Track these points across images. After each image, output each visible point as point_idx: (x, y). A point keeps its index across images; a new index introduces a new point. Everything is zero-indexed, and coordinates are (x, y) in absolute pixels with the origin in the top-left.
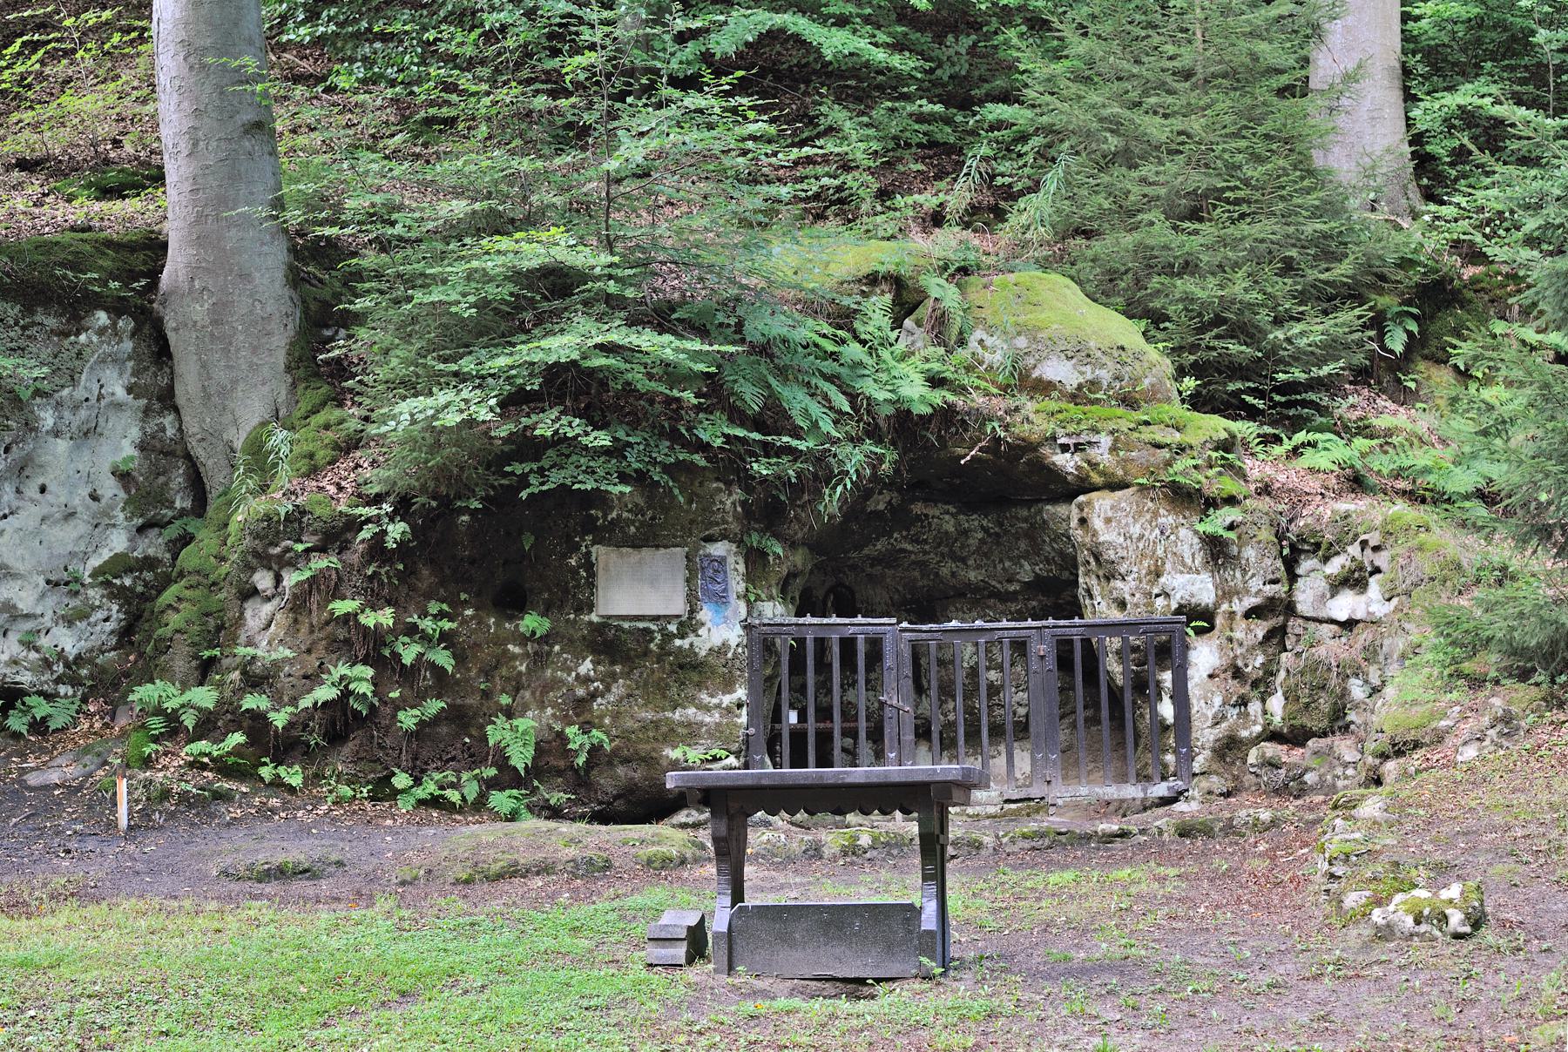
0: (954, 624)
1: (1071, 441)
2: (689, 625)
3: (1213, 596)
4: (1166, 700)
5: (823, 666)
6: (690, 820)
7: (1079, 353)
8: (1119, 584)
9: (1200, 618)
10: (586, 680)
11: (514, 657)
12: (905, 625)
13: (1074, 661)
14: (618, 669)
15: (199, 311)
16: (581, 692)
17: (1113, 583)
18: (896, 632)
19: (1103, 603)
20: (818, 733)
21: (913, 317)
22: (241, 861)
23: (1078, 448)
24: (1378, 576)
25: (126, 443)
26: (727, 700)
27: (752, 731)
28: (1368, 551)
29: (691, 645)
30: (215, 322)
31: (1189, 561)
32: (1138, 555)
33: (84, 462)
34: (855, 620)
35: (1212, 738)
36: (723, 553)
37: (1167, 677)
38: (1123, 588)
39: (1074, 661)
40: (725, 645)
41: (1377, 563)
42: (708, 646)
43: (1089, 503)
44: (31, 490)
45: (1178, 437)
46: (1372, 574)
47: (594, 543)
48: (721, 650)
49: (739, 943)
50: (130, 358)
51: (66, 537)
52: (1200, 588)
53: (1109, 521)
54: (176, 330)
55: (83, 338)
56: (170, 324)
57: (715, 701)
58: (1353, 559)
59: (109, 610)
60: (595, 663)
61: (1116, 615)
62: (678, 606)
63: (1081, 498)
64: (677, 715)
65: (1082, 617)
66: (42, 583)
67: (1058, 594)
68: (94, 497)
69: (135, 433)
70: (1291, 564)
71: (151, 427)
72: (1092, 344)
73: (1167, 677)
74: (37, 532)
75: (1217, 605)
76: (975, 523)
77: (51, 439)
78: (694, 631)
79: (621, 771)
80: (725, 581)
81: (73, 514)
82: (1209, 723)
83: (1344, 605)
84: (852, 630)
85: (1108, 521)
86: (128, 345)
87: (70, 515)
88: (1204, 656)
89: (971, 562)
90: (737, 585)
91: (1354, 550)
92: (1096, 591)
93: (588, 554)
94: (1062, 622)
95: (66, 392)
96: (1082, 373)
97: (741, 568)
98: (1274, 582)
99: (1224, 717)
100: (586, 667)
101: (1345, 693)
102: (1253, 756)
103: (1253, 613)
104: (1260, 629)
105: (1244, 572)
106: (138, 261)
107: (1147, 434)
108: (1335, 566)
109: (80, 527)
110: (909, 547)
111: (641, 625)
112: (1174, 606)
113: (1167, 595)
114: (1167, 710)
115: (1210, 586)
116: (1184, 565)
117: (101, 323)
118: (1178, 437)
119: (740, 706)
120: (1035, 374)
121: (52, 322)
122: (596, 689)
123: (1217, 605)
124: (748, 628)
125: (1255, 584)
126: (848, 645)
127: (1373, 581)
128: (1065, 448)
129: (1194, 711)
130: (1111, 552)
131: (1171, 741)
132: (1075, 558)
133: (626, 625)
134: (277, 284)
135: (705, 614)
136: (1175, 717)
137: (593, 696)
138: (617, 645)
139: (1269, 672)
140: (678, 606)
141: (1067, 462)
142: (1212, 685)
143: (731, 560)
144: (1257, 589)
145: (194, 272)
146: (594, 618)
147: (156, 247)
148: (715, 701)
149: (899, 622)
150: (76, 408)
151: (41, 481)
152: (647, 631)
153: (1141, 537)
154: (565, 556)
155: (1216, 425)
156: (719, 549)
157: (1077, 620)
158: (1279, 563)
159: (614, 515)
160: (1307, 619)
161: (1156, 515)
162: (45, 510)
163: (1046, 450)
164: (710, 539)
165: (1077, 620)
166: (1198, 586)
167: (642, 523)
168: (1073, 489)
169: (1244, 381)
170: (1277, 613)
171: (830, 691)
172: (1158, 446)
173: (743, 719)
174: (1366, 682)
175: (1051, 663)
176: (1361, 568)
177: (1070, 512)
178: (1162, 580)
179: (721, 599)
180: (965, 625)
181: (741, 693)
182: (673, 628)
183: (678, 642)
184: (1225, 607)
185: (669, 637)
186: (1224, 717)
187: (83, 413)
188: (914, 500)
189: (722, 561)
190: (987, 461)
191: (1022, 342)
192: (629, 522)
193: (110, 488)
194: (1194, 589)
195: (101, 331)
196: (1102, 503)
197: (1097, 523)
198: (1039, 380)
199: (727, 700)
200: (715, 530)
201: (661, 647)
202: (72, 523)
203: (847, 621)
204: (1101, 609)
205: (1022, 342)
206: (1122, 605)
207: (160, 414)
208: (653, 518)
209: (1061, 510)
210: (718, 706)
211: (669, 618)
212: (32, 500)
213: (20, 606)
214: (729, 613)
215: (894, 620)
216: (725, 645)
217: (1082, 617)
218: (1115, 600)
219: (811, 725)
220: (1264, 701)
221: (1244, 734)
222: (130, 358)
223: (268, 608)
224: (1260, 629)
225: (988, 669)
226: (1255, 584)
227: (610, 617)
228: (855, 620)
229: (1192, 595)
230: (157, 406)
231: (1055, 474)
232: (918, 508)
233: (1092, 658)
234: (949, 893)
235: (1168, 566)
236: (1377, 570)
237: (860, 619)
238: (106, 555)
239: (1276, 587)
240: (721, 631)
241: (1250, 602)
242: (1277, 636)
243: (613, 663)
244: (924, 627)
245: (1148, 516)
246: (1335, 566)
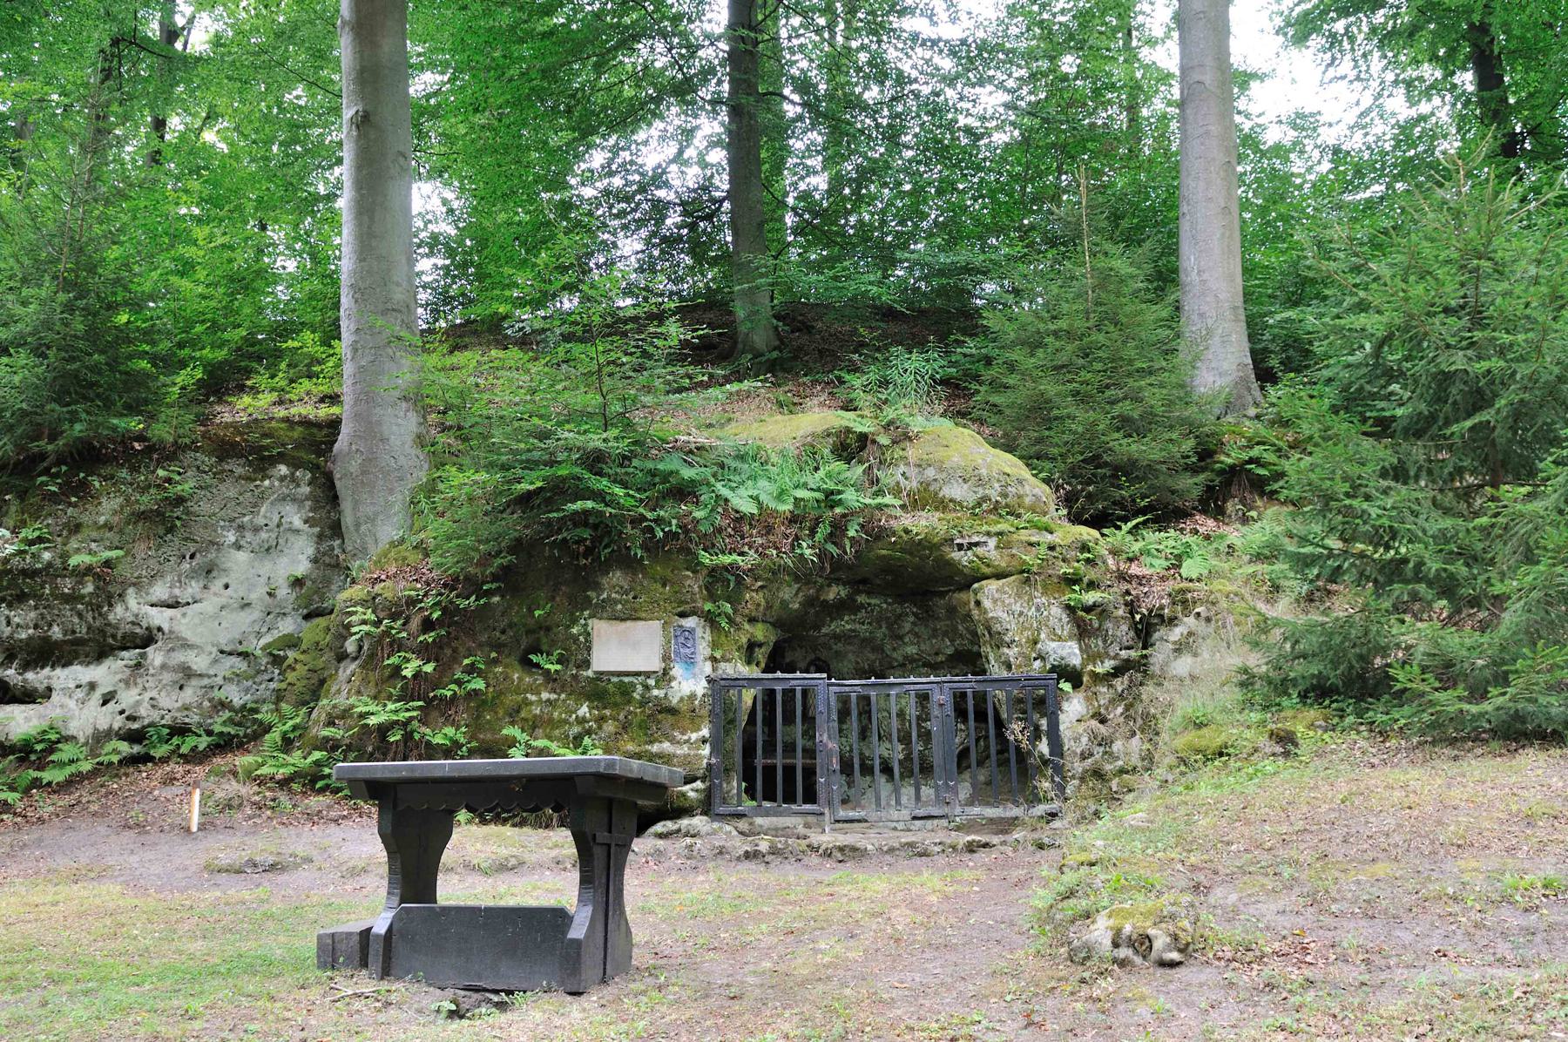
2: (665, 677)
4: (1044, 739)
6: (664, 830)
7: (973, 477)
8: (1006, 650)
11: (531, 703)
13: (974, 711)
15: (354, 466)
22: (225, 858)
25: (303, 558)
26: (694, 736)
27: (713, 761)
30: (364, 473)
32: (1024, 625)
33: (266, 568)
37: (1044, 723)
38: (1012, 653)
49: (399, 946)
50: (307, 499)
51: (245, 620)
52: (1070, 652)
53: (997, 602)
55: (267, 483)
56: (337, 476)
61: (1005, 674)
62: (655, 665)
66: (214, 650)
67: (969, 660)
69: (310, 551)
71: (324, 547)
73: (1044, 723)
74: (215, 617)
81: (248, 605)
85: (995, 601)
86: (305, 490)
87: (246, 605)
90: (703, 649)
93: (586, 625)
95: (246, 519)
100: (584, 710)
105: (1105, 641)
106: (320, 435)
109: (255, 614)
111: (626, 679)
112: (1048, 667)
113: (1043, 659)
115: (1077, 651)
121: (239, 471)
124: (710, 681)
126: (789, 694)
128: (960, 547)
133: (615, 679)
135: (677, 670)
138: (610, 693)
141: (964, 558)
143: (699, 632)
145: (356, 436)
146: (590, 673)
147: (334, 424)
150: (256, 530)
151: (225, 580)
152: (633, 685)
153: (1021, 614)
154: (569, 627)
162: (223, 601)
163: (947, 549)
169: (1104, 492)
171: (755, 724)
181: (705, 732)
183: (655, 692)
185: (647, 688)
187: (264, 535)
188: (859, 592)
189: (692, 631)
192: (616, 602)
193: (284, 591)
194: (1064, 653)
195: (282, 479)
196: (991, 586)
197: (987, 604)
199: (694, 736)
201: (643, 696)
202: (248, 610)
205: (930, 473)
206: (1009, 667)
207: (331, 538)
209: (963, 596)
211: (648, 674)
213: (195, 667)
222: (307, 499)
223: (353, 666)
230: (328, 532)
232: (861, 599)
235: (1043, 636)
237: (798, 675)
238: (276, 634)
240: (689, 684)
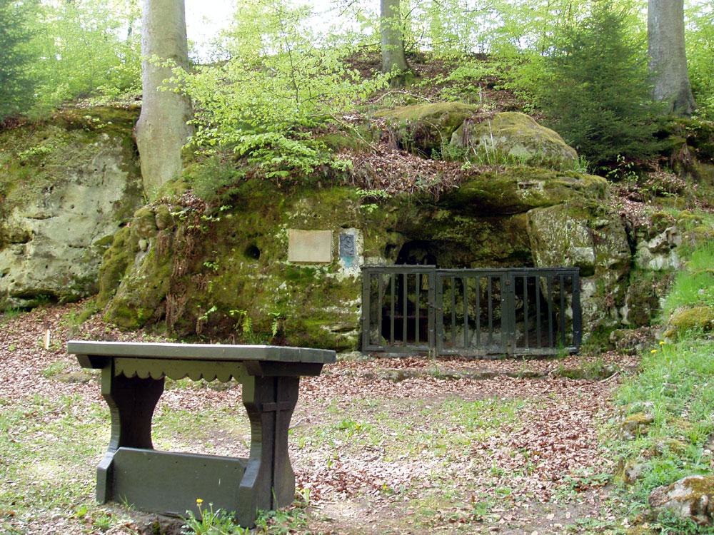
1: (524, 183)
2: (334, 267)
4: (570, 308)
7: (528, 143)
9: (586, 270)
20: (396, 320)
21: (456, 131)
24: (675, 249)
36: (352, 234)
37: (570, 297)
39: (525, 287)
40: (352, 278)
42: (343, 277)
44: (67, 206)
46: (672, 247)
47: (288, 227)
50: (121, 154)
54: (140, 142)
55: (96, 144)
56: (138, 141)
57: (347, 303)
59: (101, 258)
63: (530, 211)
64: (328, 309)
66: (66, 245)
68: (100, 211)
69: (123, 186)
73: (570, 297)
77: (76, 186)
80: (353, 246)
83: (658, 262)
84: (413, 270)
86: (120, 149)
88: (589, 287)
96: (531, 153)
97: (362, 241)
99: (598, 317)
100: (284, 285)
106: (128, 116)
108: (654, 243)
114: (569, 312)
117: (105, 139)
127: (672, 251)
131: (572, 328)
134: (179, 122)
135: (341, 262)
136: (573, 316)
140: (327, 257)
142: (592, 300)
148: (347, 303)
151: (72, 203)
152: (313, 270)
155: (599, 180)
156: (350, 232)
159: (297, 214)
164: (346, 227)
167: (310, 218)
168: (525, 208)
170: (628, 268)
173: (359, 312)
176: (667, 244)
177: (524, 217)
179: (350, 256)
181: (359, 300)
186: (598, 317)
189: (351, 237)
191: (504, 139)
195: (105, 142)
196: (541, 212)
200: (349, 223)
207: (135, 178)
208: (315, 216)
210: (348, 306)
212: (66, 211)
214: (354, 262)
216: (352, 278)
219: (405, 317)
221: (608, 325)
222: (121, 154)
225: (493, 293)
227: (295, 263)
232: (457, 218)
234: (275, 471)
239: (625, 254)
240: (349, 271)
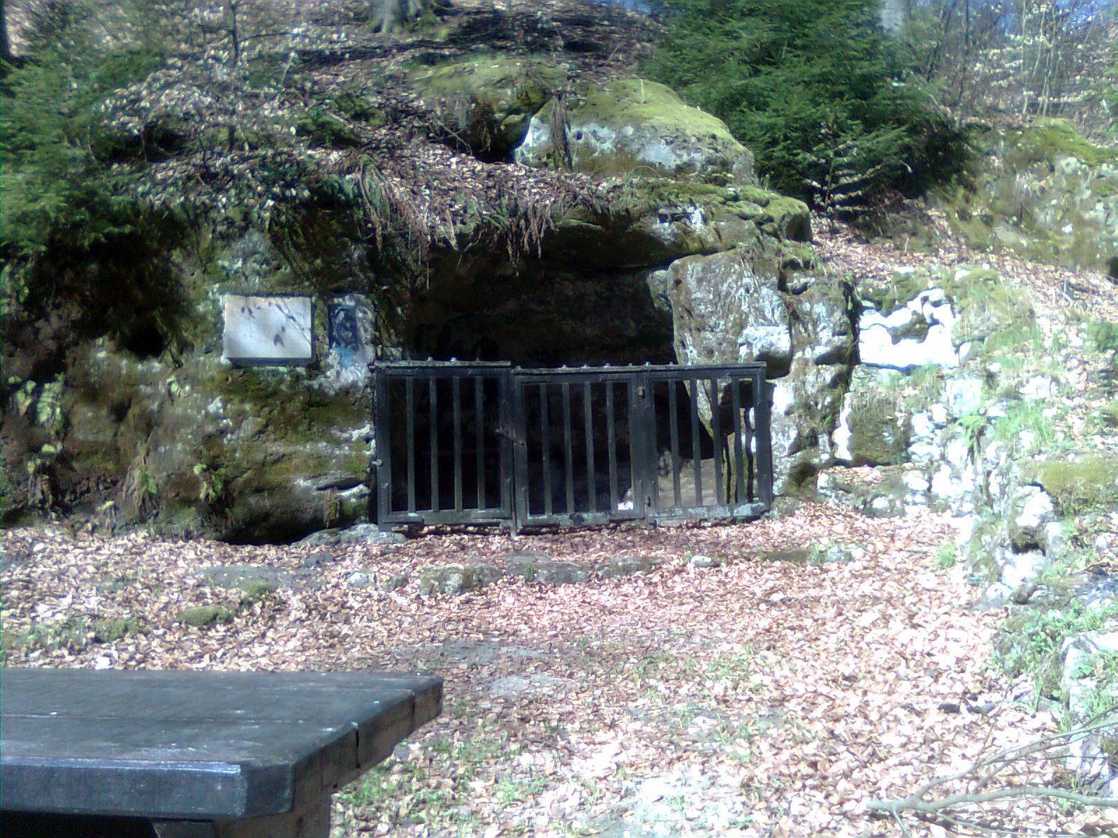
0: (564, 368)
3: (788, 345)
5: (468, 402)
7: (677, 140)
9: (777, 365)
10: (216, 418)
12: (519, 368)
14: (248, 407)
16: (210, 429)
17: (703, 334)
18: (517, 375)
19: (695, 352)
23: (675, 218)
27: (378, 462)
28: (927, 305)
29: (320, 385)
31: (769, 316)
34: (474, 363)
35: (788, 465)
41: (935, 317)
43: (683, 266)
45: (761, 211)
48: (346, 391)
52: (780, 340)
57: (346, 435)
58: (914, 313)
60: (225, 403)
61: (703, 361)
63: (677, 262)
65: (676, 363)
70: (854, 314)
72: (688, 132)
75: (792, 353)
76: (591, 288)
78: (323, 373)
79: (252, 500)
82: (786, 453)
83: (909, 351)
84: (470, 371)
88: (783, 395)
89: (587, 321)
91: (915, 305)
92: (689, 340)
94: (658, 367)
98: (841, 334)
100: (215, 406)
101: (908, 427)
102: (823, 479)
103: (822, 360)
104: (829, 373)
107: (735, 208)
108: (901, 318)
110: (536, 308)
112: (756, 352)
116: (765, 318)
118: (761, 211)
119: (368, 440)
120: (640, 157)
122: (227, 426)
123: (792, 353)
125: (825, 335)
128: (663, 218)
129: (773, 442)
130: (702, 307)
132: (671, 316)
137: (223, 432)
139: (834, 409)
141: (664, 230)
144: (827, 340)
149: (513, 367)
157: (671, 365)
158: (846, 319)
160: (869, 365)
161: (741, 276)
165: (671, 365)
166: (776, 336)
168: (665, 254)
172: (745, 217)
174: (930, 419)
175: (648, 404)
178: (745, 332)
180: (573, 370)
181: (367, 429)
182: (301, 370)
183: (306, 382)
184: (798, 355)
190: (597, 232)
197: (691, 282)
198: (643, 162)
199: (356, 434)
203: (467, 363)
204: (691, 354)
215: (509, 364)
217: (676, 363)
218: (705, 348)
220: (830, 434)
224: (829, 373)
226: (825, 335)
228: (474, 363)
229: (772, 345)
231: (653, 241)
233: (686, 405)
235: (751, 319)
236: (935, 322)
239: (844, 338)
240: (350, 372)
241: (821, 350)
242: (842, 381)
243: (242, 401)
244: (535, 371)
245: (734, 277)
246: (901, 318)
